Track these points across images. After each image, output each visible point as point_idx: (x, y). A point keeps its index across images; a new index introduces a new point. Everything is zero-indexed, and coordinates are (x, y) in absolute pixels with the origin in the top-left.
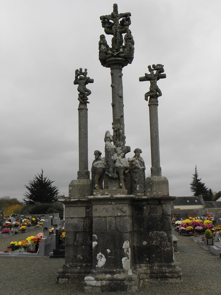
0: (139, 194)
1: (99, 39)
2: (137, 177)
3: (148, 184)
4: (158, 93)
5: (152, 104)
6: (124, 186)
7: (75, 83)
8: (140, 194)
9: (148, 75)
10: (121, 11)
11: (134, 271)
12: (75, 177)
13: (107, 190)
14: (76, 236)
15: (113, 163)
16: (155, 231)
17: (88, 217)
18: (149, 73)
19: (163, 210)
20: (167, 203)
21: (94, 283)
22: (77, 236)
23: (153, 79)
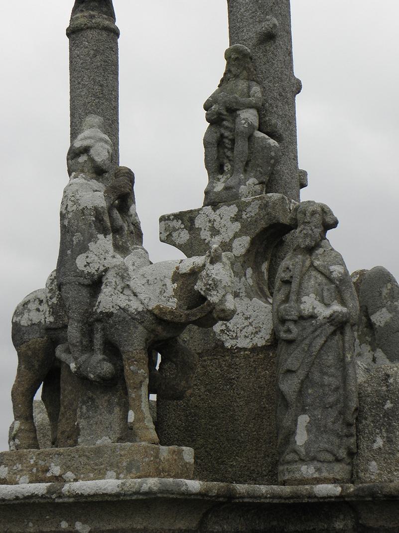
0: (307, 470)
2: (289, 371)
13: (60, 454)
15: (85, 292)
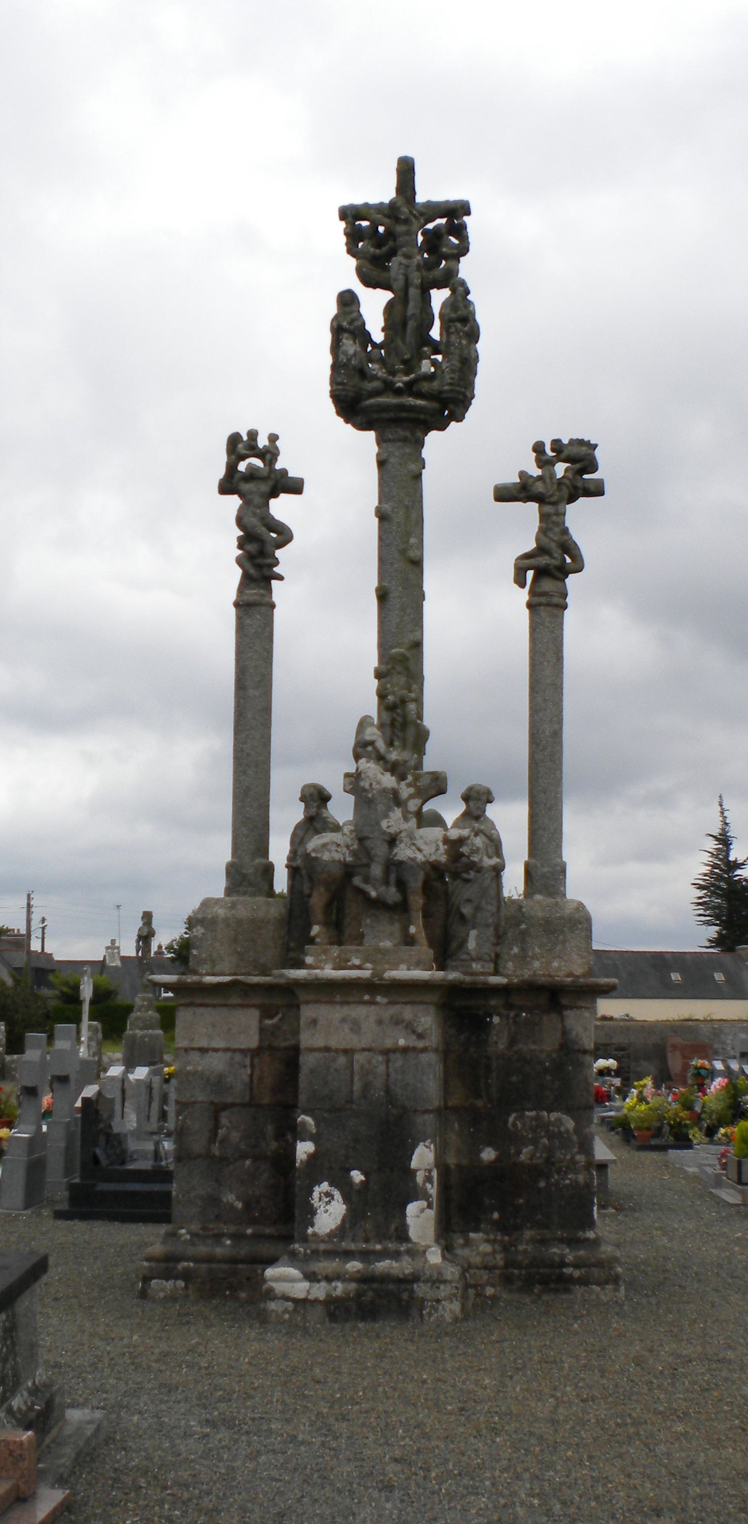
0: (476, 966)
1: (332, 309)
3: (510, 924)
4: (568, 560)
5: (540, 604)
6: (422, 937)
7: (227, 486)
8: (479, 966)
9: (531, 481)
10: (427, 191)
11: (447, 1256)
12: (217, 888)
14: (216, 1119)
16: (529, 1110)
17: (271, 1048)
18: (536, 472)
19: (565, 1032)
20: (584, 1005)
21: (300, 1289)
22: (224, 1121)
23: (552, 500)
